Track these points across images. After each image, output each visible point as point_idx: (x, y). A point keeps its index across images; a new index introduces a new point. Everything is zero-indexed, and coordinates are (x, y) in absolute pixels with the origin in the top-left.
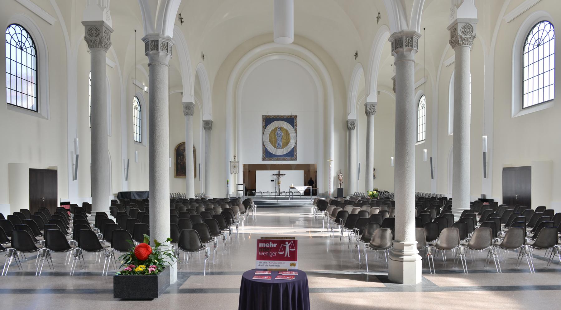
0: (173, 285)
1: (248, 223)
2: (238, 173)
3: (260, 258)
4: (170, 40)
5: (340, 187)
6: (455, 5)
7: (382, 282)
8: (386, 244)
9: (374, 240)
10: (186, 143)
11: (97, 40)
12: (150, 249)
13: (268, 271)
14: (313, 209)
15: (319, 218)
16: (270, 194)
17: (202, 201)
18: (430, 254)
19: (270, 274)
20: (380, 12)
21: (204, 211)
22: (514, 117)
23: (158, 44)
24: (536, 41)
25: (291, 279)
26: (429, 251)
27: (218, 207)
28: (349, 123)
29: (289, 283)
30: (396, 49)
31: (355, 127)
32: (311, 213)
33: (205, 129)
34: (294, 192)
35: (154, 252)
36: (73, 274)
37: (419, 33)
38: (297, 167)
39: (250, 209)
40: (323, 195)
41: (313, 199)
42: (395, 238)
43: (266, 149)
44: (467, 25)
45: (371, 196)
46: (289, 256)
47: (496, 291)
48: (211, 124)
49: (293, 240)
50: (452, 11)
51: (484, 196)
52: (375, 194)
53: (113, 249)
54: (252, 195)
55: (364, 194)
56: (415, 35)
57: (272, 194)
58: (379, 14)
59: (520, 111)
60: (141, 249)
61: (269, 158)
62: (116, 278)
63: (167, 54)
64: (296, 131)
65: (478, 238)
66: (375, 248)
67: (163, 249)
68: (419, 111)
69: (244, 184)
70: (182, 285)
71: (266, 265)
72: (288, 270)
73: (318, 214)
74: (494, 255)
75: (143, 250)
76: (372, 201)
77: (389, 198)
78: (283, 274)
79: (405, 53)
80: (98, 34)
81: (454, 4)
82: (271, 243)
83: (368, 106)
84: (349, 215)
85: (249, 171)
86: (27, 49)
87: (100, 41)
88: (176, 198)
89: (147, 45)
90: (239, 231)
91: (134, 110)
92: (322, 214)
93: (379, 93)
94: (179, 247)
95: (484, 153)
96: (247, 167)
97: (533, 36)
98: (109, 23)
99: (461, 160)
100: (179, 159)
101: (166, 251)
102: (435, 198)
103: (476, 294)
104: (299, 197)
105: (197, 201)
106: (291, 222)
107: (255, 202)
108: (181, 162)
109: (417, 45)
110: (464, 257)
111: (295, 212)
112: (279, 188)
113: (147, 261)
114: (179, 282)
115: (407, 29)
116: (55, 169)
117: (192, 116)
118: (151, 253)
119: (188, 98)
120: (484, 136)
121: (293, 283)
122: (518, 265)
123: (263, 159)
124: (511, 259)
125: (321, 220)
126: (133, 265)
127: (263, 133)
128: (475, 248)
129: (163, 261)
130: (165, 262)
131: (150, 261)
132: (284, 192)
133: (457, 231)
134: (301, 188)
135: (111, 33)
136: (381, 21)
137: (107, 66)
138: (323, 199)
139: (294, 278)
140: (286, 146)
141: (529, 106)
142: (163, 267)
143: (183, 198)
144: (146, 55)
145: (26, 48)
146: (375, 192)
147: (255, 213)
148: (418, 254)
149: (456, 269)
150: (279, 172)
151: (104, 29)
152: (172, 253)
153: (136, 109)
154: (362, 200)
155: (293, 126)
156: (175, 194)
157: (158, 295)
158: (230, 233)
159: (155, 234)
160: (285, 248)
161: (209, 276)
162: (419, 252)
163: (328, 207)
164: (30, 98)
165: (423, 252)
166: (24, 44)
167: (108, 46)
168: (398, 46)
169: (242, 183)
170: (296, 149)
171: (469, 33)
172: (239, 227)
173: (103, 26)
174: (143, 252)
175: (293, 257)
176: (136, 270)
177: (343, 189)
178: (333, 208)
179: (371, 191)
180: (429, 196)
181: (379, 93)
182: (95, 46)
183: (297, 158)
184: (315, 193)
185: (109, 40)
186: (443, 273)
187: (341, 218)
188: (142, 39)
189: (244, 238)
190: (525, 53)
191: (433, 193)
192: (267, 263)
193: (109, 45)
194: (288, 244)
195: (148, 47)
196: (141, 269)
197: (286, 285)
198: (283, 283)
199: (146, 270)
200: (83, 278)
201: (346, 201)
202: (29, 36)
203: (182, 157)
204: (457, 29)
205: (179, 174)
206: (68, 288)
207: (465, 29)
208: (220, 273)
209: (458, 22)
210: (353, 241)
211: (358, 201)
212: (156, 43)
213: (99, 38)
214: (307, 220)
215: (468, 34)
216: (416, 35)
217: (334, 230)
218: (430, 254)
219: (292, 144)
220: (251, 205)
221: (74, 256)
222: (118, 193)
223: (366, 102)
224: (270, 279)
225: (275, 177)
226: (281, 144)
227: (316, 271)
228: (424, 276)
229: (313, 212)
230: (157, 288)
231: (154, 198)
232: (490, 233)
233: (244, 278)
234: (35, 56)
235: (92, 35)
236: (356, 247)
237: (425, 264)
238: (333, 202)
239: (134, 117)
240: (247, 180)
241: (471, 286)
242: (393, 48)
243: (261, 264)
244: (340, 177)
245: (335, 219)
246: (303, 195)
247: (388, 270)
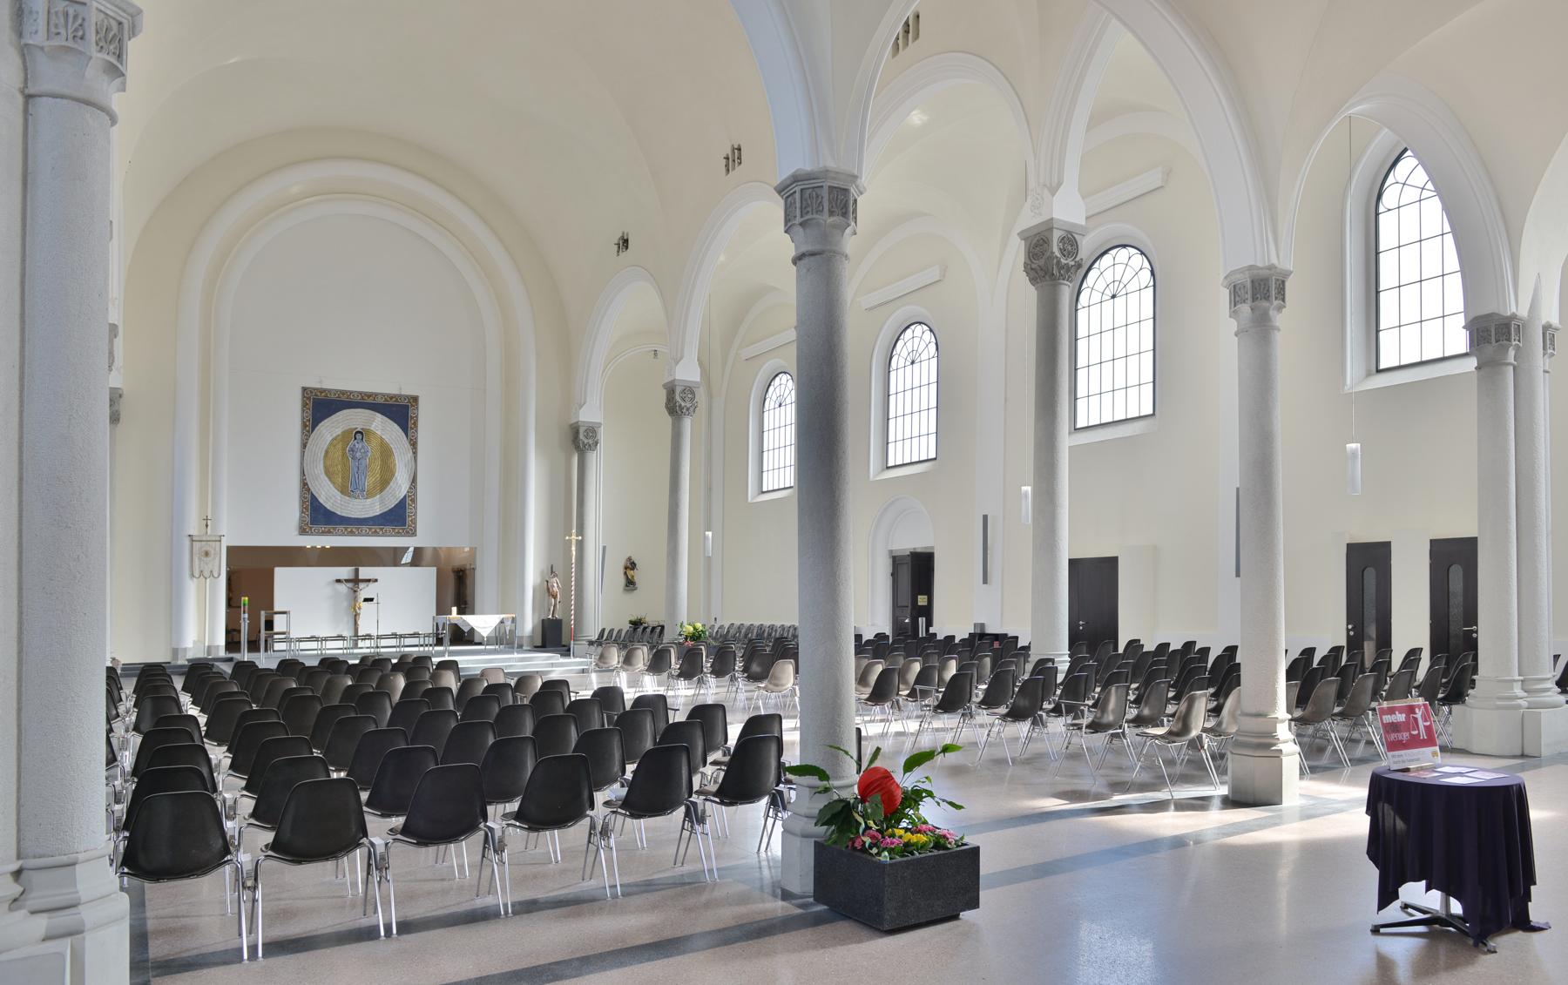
5: (553, 616)
28: (582, 431)
31: (597, 443)
43: (313, 497)
51: (982, 625)
61: (323, 528)
64: (414, 444)
68: (766, 414)
120: (1024, 488)
127: (304, 446)
140: (381, 491)
150: (357, 571)
155: (405, 429)
170: (414, 501)
183: (415, 528)
190: (1079, 307)
226: (370, 481)
231: (836, 638)
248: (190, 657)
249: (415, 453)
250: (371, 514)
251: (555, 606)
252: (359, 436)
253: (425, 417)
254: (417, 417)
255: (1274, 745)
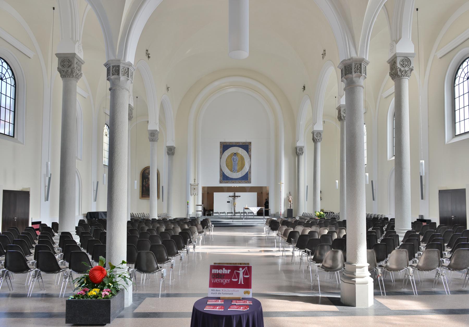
0: (128, 308)
1: (205, 242)
2: (196, 195)
3: (213, 285)
4: (131, 66)
5: (290, 208)
6: (394, 41)
7: (335, 305)
8: (338, 266)
9: (325, 262)
10: (150, 167)
11: (69, 70)
12: (105, 272)
13: (221, 300)
14: (266, 228)
15: (271, 237)
16: (226, 214)
17: (164, 221)
18: (380, 275)
19: (223, 303)
20: (325, 49)
21: (164, 231)
22: (448, 143)
23: (119, 69)
24: (466, 74)
25: (245, 310)
26: (379, 273)
27: (177, 227)
28: (298, 149)
29: (243, 315)
30: (345, 76)
31: (303, 153)
32: (264, 232)
33: (168, 154)
34: (248, 213)
35: (108, 274)
36: (30, 296)
37: (367, 60)
38: (251, 189)
39: (208, 229)
40: (274, 216)
41: (265, 219)
42: (348, 260)
43: (223, 173)
44: (406, 58)
45: (318, 217)
46: (242, 283)
47: (449, 315)
48: (174, 150)
49: (247, 265)
50: (392, 46)
51: (422, 216)
52: (322, 215)
53: (71, 270)
54: (209, 215)
55: (311, 214)
56: (363, 62)
57: (229, 215)
58: (324, 51)
59: (453, 138)
60: (96, 272)
61: (226, 181)
62: (68, 302)
63: (127, 79)
64: (250, 156)
65: (426, 259)
66: (327, 269)
67: (119, 272)
69: (203, 205)
70: (137, 308)
71: (219, 293)
72: (242, 299)
73: (270, 233)
74: (442, 277)
75: (98, 273)
76: (320, 221)
77: (335, 218)
78: (236, 304)
79: (354, 79)
80: (70, 65)
81: (393, 40)
82: (224, 269)
83: (315, 134)
84: (300, 236)
85: (208, 193)
86: (7, 79)
87: (72, 71)
88: (140, 218)
89: (108, 70)
90: (197, 251)
91: (104, 137)
92: (274, 234)
93: (324, 122)
94: (136, 268)
95: (421, 177)
96: (206, 190)
97: (463, 70)
98: (80, 55)
99: (403, 183)
100: (144, 182)
101: (120, 274)
102: (377, 218)
103: (431, 319)
104: (253, 217)
105: (159, 221)
106: (245, 241)
107: (212, 221)
108: (146, 184)
109: (365, 71)
110: (413, 278)
111: (249, 232)
112: (235, 209)
113: (101, 284)
114: (134, 304)
115: (356, 56)
116: (28, 191)
117: (156, 142)
118: (106, 275)
119: (154, 125)
120: (421, 161)
121: (247, 315)
122: (464, 286)
123: (221, 182)
124: (456, 280)
125: (273, 239)
126: (87, 289)
127: (221, 158)
128: (423, 269)
129: (117, 284)
130: (120, 285)
131: (104, 285)
132: (239, 213)
133: (406, 252)
134: (255, 209)
135: (82, 65)
136: (326, 57)
137: (77, 95)
138: (275, 219)
139: (248, 309)
140: (241, 170)
141: (461, 133)
142: (117, 291)
143: (147, 218)
144: (108, 79)
145: (6, 79)
146: (322, 213)
147: (213, 232)
148: (370, 276)
149: (406, 290)
150: (235, 194)
151: (76, 61)
152: (127, 275)
153: (106, 136)
154: (311, 221)
155: (248, 152)
156: (140, 214)
157: (111, 320)
158: (187, 253)
159: (111, 256)
160: (238, 274)
161: (165, 298)
162: (370, 274)
163: (280, 227)
164: (7, 124)
165: (374, 274)
166: (4, 75)
167: (79, 76)
168: (347, 73)
169: (201, 204)
170: (250, 173)
171: (407, 66)
172: (197, 247)
173: (75, 58)
174: (98, 275)
175: (247, 284)
176: (89, 294)
177: (292, 209)
178: (285, 228)
179: (318, 212)
180: (371, 217)
181: (324, 122)
182: (67, 76)
184: (267, 213)
185: (80, 70)
186: (393, 295)
187: (293, 239)
188: (104, 65)
189: (201, 257)
190: (455, 85)
191: (375, 214)
192: (219, 291)
193: (80, 75)
194: (242, 270)
195: (110, 72)
196: (94, 293)
197: (239, 317)
198: (236, 316)
199: (100, 293)
200: (41, 300)
201: (296, 221)
202: (9, 68)
203: (147, 179)
204: (396, 63)
205: (144, 195)
206: (25, 312)
207: (404, 62)
208: (176, 295)
209: (397, 56)
210: (304, 260)
211: (307, 221)
212: (117, 68)
213: (71, 69)
214: (260, 239)
215: (406, 67)
216: (365, 62)
217: (286, 249)
218: (380, 275)
219: (246, 169)
220: (209, 225)
221: (33, 278)
222: (87, 213)
223: (313, 130)
224: (223, 310)
225: (231, 199)
226: (237, 168)
227: (269, 292)
228: (375, 299)
229: (266, 232)
230: (110, 313)
232: (437, 254)
233: (195, 308)
234: (14, 86)
235: (64, 66)
236: (308, 267)
237: (376, 286)
238: (285, 223)
239: (104, 143)
240: (206, 201)
241: (423, 309)
242: (343, 74)
243: (213, 292)
244: (290, 199)
245: (287, 239)
246: (257, 215)
247: (339, 291)
248: (191, 217)
249: (250, 159)
250: (238, 177)
251: (290, 205)
252: (235, 155)
253: (253, 149)
254: (251, 148)
255: (354, 278)
